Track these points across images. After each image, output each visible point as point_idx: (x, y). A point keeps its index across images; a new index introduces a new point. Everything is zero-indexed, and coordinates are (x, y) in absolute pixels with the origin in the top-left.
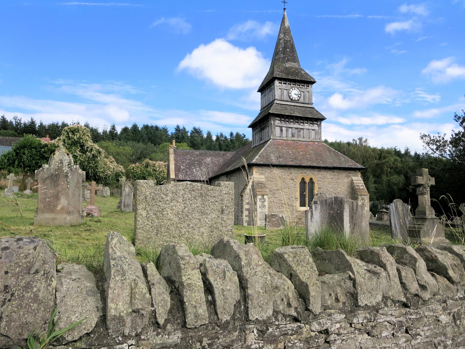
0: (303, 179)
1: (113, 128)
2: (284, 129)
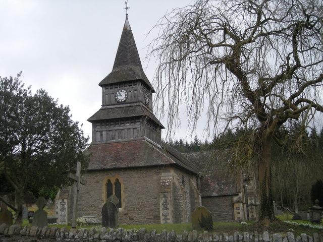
0: (109, 181)
1: (177, 141)
2: (104, 133)
